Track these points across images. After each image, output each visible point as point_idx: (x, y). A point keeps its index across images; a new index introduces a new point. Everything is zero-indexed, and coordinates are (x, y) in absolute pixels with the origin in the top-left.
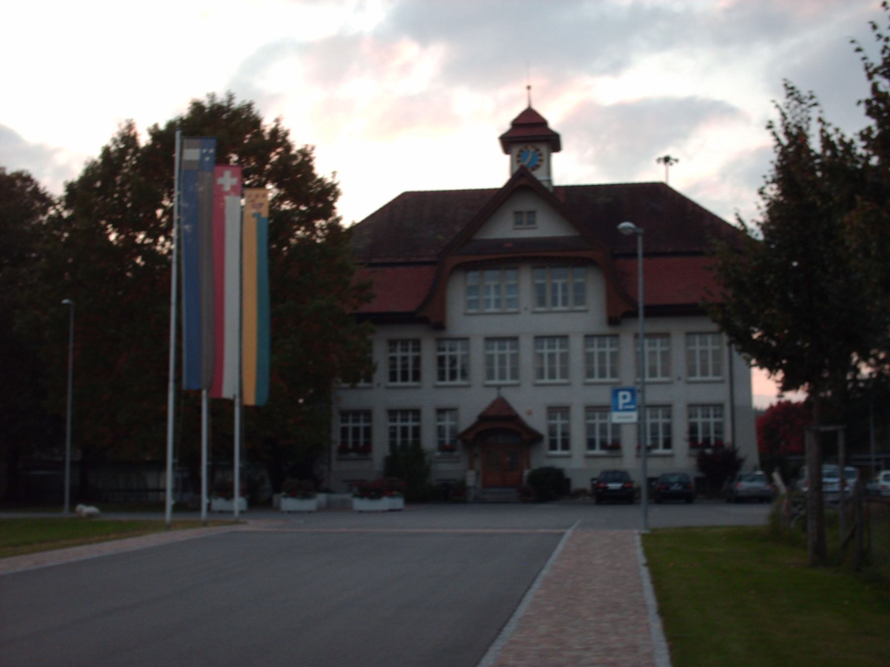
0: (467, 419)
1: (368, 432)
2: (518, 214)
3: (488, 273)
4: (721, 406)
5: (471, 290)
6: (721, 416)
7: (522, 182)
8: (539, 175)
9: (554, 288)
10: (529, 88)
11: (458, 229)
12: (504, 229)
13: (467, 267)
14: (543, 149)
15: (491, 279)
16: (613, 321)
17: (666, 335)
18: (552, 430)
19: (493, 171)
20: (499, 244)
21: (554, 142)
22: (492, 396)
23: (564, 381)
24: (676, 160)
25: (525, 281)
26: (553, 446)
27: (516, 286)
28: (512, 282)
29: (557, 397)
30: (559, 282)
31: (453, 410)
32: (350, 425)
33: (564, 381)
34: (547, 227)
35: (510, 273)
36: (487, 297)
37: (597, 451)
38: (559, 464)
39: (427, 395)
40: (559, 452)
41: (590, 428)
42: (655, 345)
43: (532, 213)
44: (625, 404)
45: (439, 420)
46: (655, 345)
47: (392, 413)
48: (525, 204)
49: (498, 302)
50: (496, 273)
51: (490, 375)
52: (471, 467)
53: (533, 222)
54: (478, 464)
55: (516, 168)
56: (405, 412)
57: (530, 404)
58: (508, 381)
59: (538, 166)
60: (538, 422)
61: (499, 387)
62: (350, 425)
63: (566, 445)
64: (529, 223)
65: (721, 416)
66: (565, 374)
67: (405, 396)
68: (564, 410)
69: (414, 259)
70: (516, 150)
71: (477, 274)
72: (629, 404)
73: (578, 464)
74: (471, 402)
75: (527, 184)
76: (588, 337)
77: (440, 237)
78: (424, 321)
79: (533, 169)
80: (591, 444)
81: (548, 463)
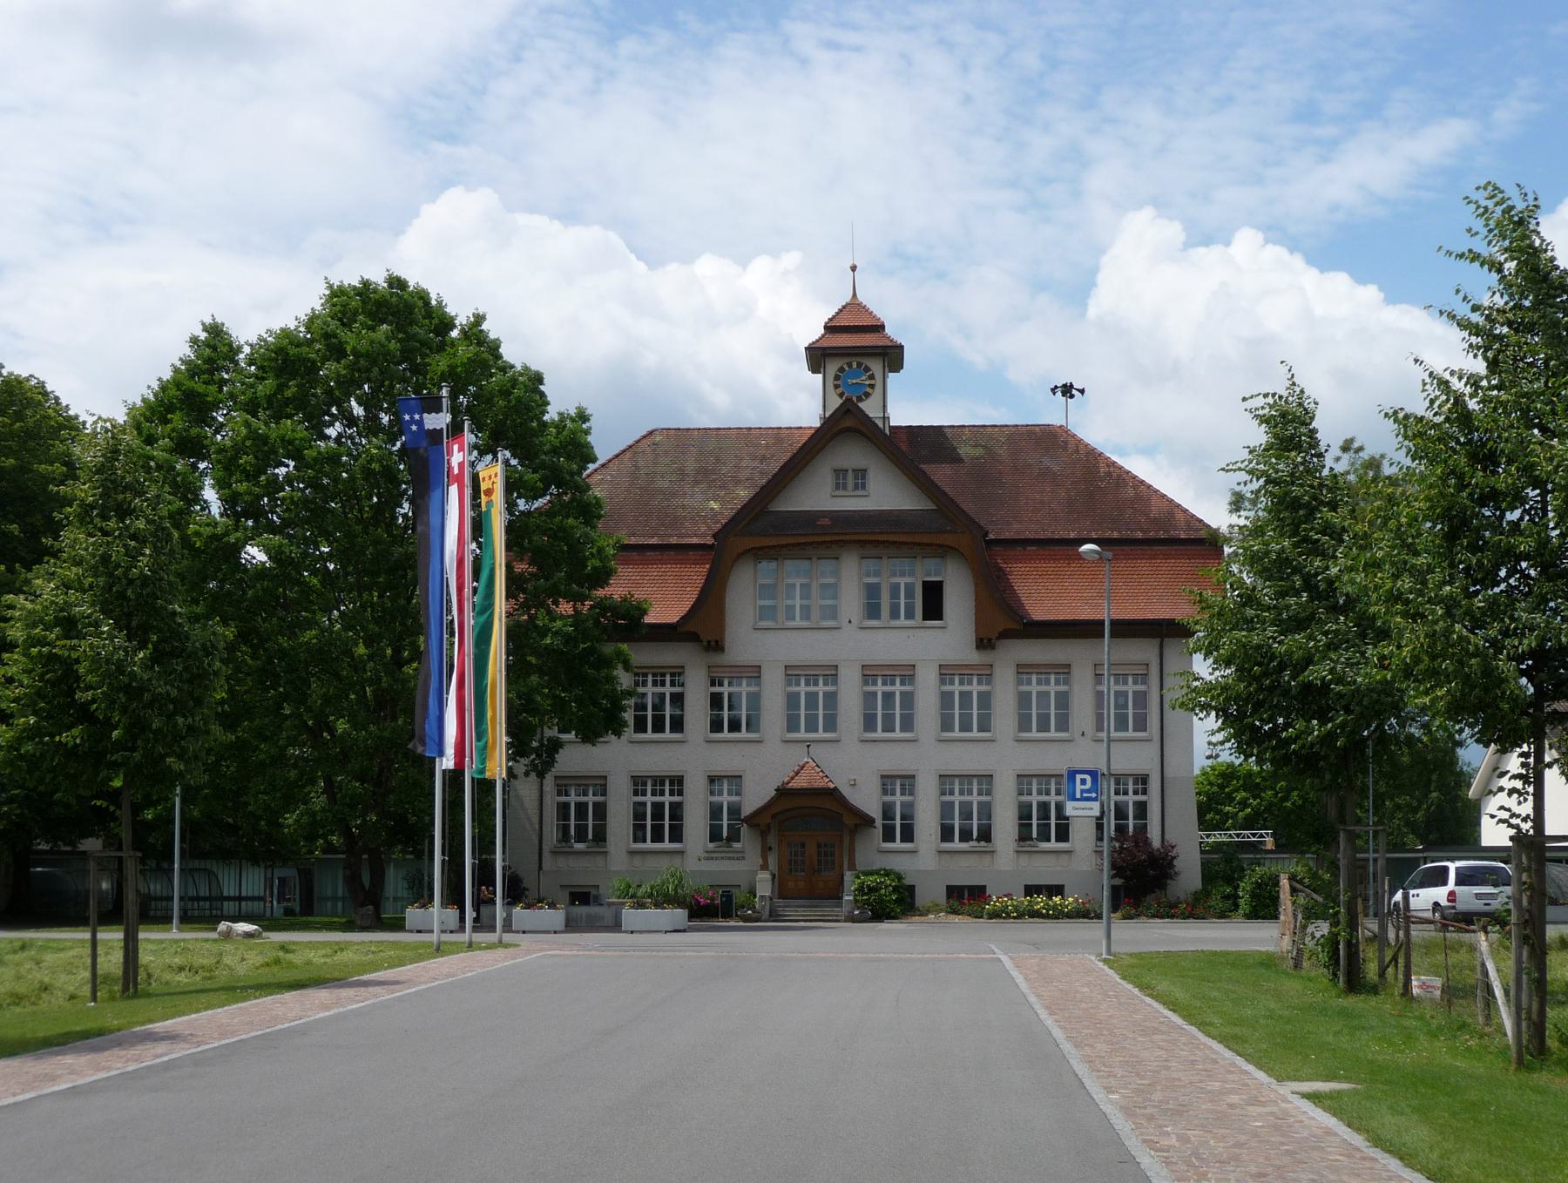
0: (755, 796)
1: (601, 811)
2: (840, 473)
3: (790, 565)
4: (1143, 780)
5: (768, 591)
6: (1145, 792)
7: (848, 422)
8: (870, 408)
9: (895, 590)
10: (854, 268)
11: (744, 494)
12: (817, 495)
13: (759, 554)
14: (876, 366)
15: (794, 575)
16: (984, 643)
17: (1064, 670)
18: (888, 812)
19: (801, 402)
20: (809, 520)
21: (892, 356)
22: (798, 756)
23: (805, 624)
24: (1082, 391)
25: (850, 577)
26: (889, 835)
27: (834, 586)
28: (832, 580)
29: (895, 759)
30: (902, 581)
31: (736, 779)
32: (573, 799)
33: (805, 624)
34: (886, 493)
35: (827, 565)
36: (789, 602)
37: (957, 845)
38: (898, 864)
39: (693, 754)
40: (898, 845)
41: (946, 808)
42: (1048, 683)
43: (861, 473)
44: (1083, 791)
45: (712, 793)
46: (1048, 683)
47: (639, 783)
48: (851, 455)
49: (806, 614)
50: (804, 565)
51: (792, 725)
52: (764, 867)
53: (863, 487)
54: (772, 860)
55: (836, 402)
56: (659, 781)
57: (854, 767)
58: (821, 735)
59: (867, 395)
60: (867, 800)
61: (809, 744)
62: (573, 799)
63: (908, 835)
64: (856, 487)
65: (1145, 792)
66: (907, 724)
67: (727, 756)
68: (908, 781)
69: (674, 540)
70: (832, 367)
71: (773, 565)
72: (1088, 791)
73: (925, 861)
74: (765, 766)
75: (848, 424)
76: (946, 672)
77: (714, 505)
78: (693, 637)
79: (860, 399)
80: (946, 833)
81: (880, 862)
